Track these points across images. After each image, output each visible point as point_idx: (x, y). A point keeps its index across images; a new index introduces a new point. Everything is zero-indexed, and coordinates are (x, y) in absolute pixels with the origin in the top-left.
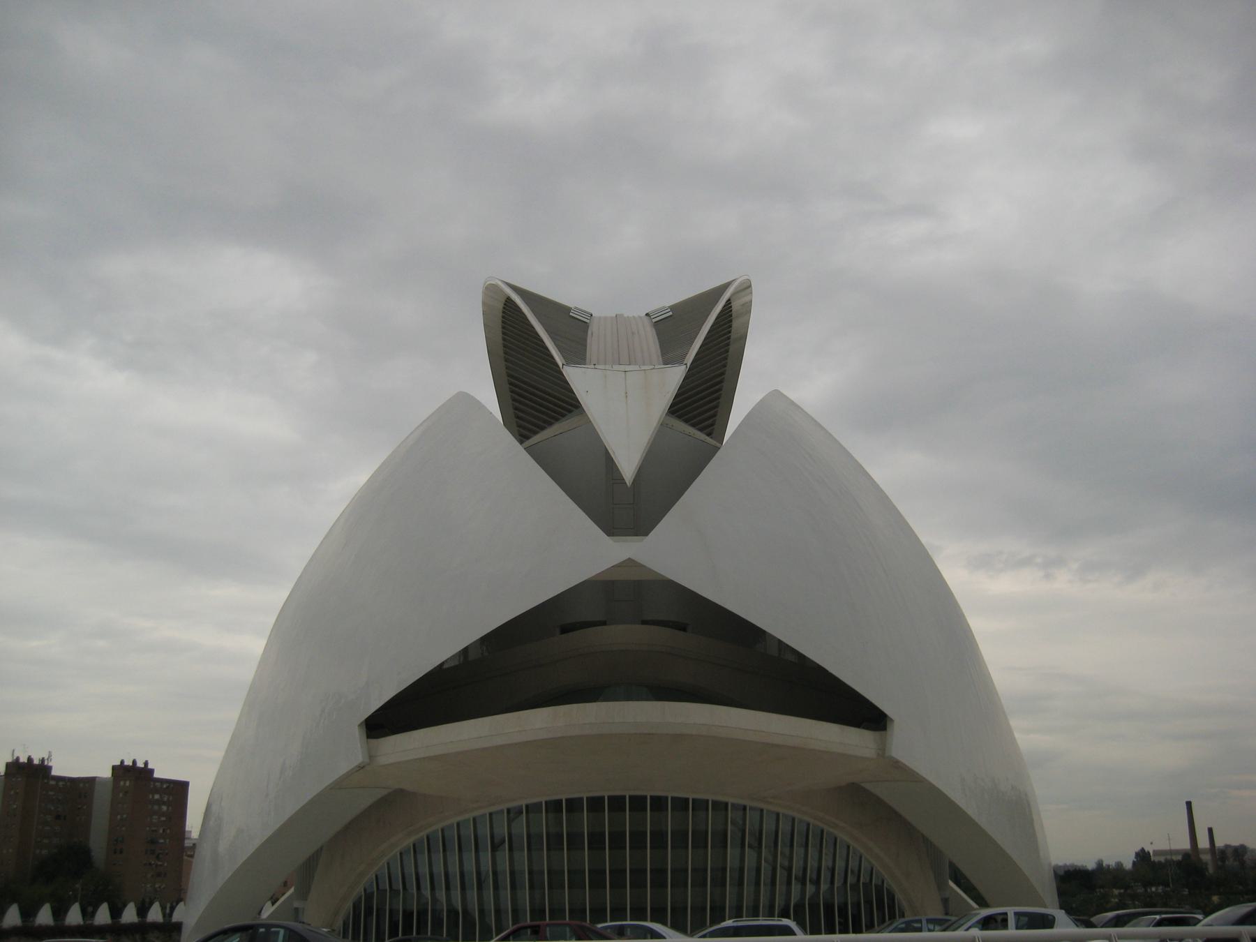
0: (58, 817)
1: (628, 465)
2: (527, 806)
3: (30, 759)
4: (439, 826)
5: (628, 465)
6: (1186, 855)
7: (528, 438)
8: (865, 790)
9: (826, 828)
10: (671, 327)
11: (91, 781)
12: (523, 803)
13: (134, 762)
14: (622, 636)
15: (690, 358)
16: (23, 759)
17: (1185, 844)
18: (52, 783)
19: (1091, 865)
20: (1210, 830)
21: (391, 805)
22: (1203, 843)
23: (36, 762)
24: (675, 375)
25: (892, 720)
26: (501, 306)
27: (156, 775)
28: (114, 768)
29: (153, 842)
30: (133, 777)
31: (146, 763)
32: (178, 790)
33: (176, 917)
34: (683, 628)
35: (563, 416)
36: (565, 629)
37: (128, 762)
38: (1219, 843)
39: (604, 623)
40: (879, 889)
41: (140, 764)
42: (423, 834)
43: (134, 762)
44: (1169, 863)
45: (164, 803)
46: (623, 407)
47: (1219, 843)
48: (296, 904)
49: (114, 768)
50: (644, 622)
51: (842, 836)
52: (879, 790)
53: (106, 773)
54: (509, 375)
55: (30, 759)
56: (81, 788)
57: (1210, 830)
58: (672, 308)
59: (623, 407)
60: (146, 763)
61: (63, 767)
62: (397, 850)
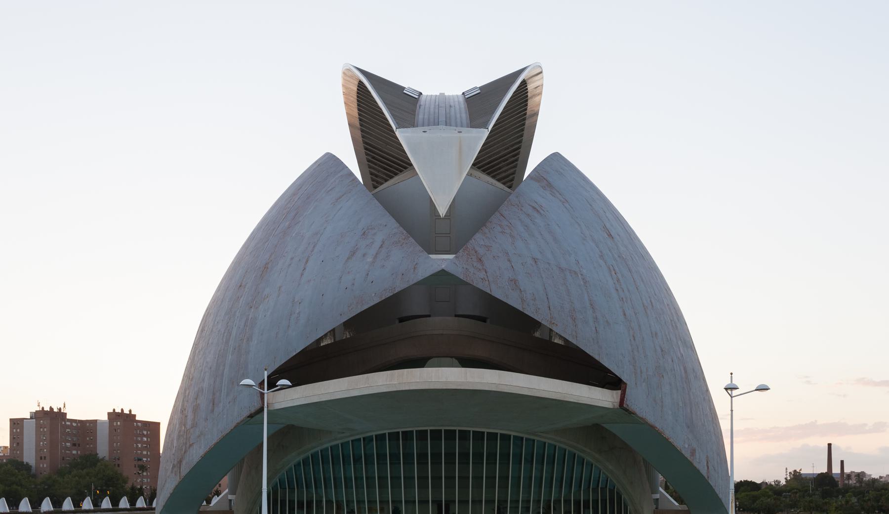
0: (74, 445)
1: (442, 211)
2: (376, 436)
3: (51, 408)
4: (319, 449)
5: (442, 211)
6: (821, 476)
7: (375, 187)
8: (603, 427)
9: (577, 453)
10: (479, 102)
11: (94, 422)
12: (374, 434)
13: (122, 410)
14: (442, 324)
15: (490, 128)
16: (47, 409)
17: (824, 470)
18: (68, 423)
19: (759, 482)
20: (842, 462)
21: (289, 431)
22: (836, 470)
23: (56, 410)
24: (482, 135)
25: (626, 384)
26: (355, 89)
27: (137, 418)
28: (109, 414)
29: (140, 460)
30: (122, 420)
31: (130, 411)
32: (154, 427)
33: (154, 505)
34: (483, 320)
35: (401, 171)
36: (402, 320)
37: (118, 410)
38: (847, 470)
39: (429, 316)
40: (612, 491)
41: (126, 411)
42: (309, 454)
43: (122, 410)
44: (810, 479)
45: (145, 436)
46: (442, 168)
47: (847, 470)
48: (230, 497)
49: (109, 414)
50: (456, 316)
51: (587, 458)
52: (616, 429)
53: (105, 418)
54: (365, 142)
55: (51, 408)
56: (87, 428)
57: (842, 462)
58: (481, 88)
59: (442, 168)
60: (130, 411)
61: (74, 413)
62: (292, 464)
